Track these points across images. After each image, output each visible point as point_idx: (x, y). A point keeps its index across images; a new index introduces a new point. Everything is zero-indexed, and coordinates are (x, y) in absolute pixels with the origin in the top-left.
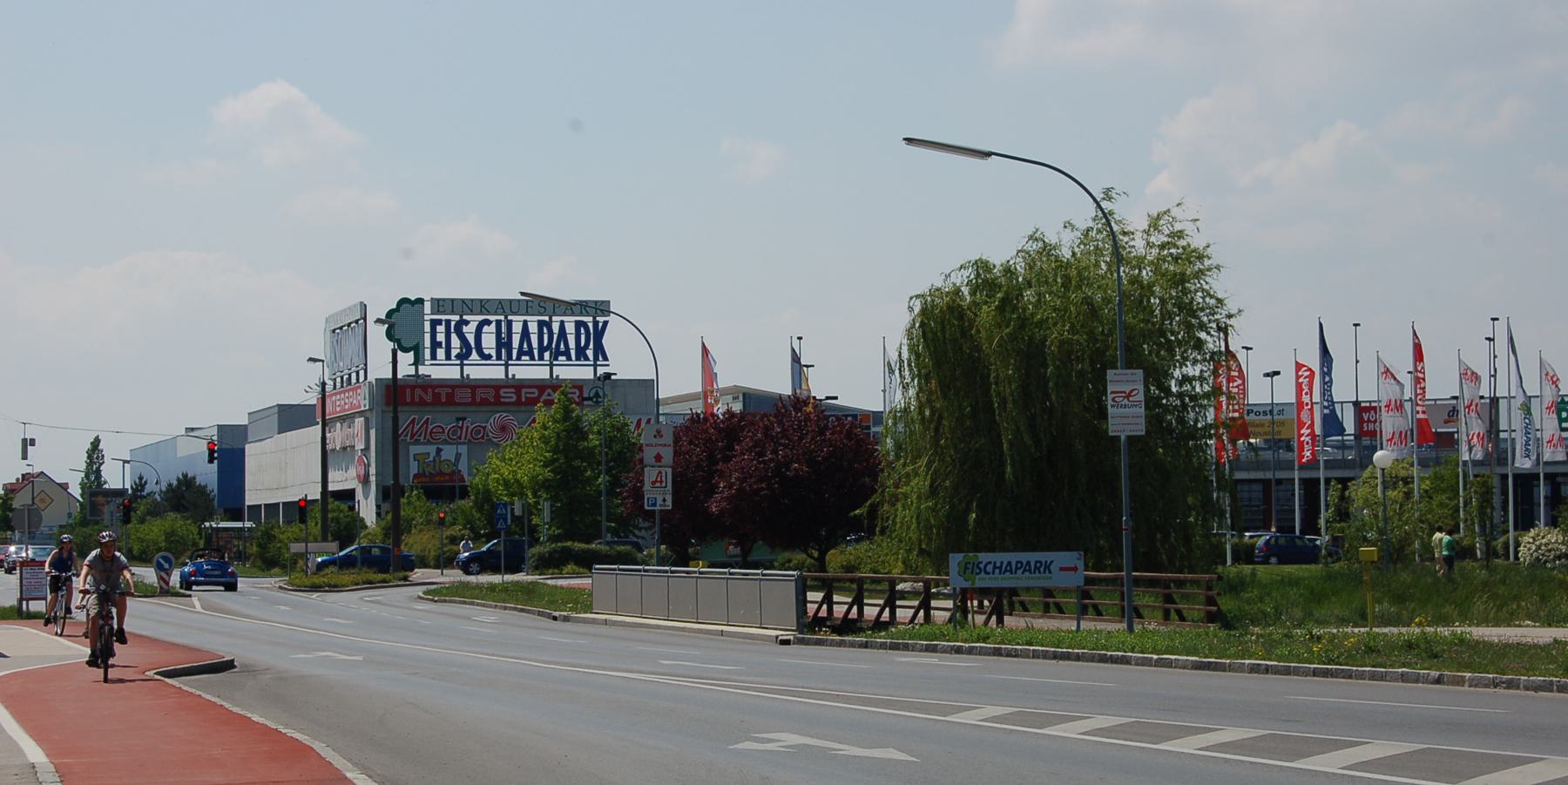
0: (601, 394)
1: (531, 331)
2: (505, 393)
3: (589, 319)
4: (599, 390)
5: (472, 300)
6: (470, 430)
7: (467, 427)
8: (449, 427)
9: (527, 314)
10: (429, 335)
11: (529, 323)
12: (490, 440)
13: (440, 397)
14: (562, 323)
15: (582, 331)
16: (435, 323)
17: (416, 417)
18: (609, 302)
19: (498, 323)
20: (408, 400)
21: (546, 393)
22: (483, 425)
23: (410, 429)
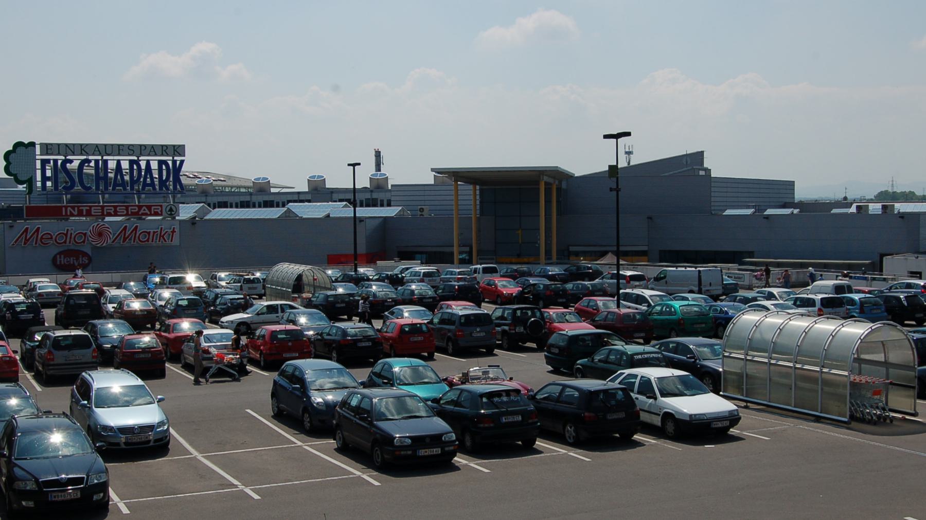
0: (174, 210)
1: (152, 168)
2: (135, 209)
3: (169, 159)
4: (173, 207)
5: (74, 145)
6: (73, 236)
7: (71, 234)
8: (56, 234)
9: (119, 155)
10: (40, 171)
11: (121, 162)
12: (90, 243)
13: (83, 212)
14: (148, 162)
15: (164, 167)
16: (44, 163)
17: (128, 225)
18: (184, 145)
19: (97, 161)
20: (64, 214)
21: (143, 209)
22: (84, 232)
23: (24, 236)
